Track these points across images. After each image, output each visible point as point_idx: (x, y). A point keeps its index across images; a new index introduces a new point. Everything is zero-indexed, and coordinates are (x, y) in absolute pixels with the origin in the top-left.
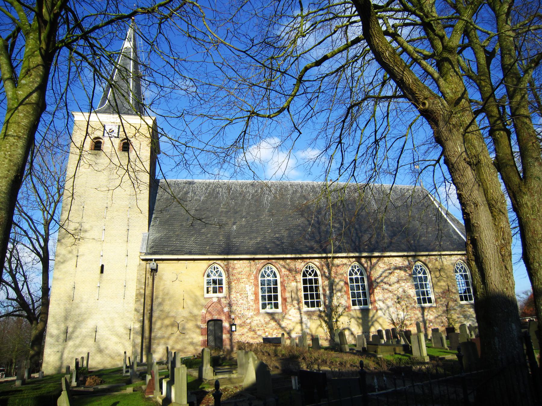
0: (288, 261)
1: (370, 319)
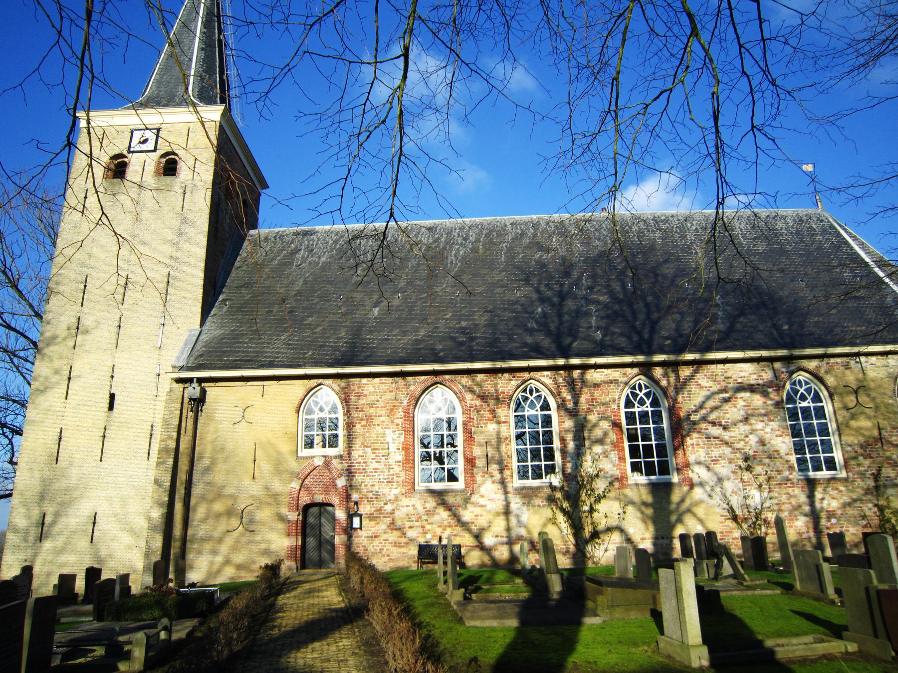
0: (480, 377)
1: (673, 506)
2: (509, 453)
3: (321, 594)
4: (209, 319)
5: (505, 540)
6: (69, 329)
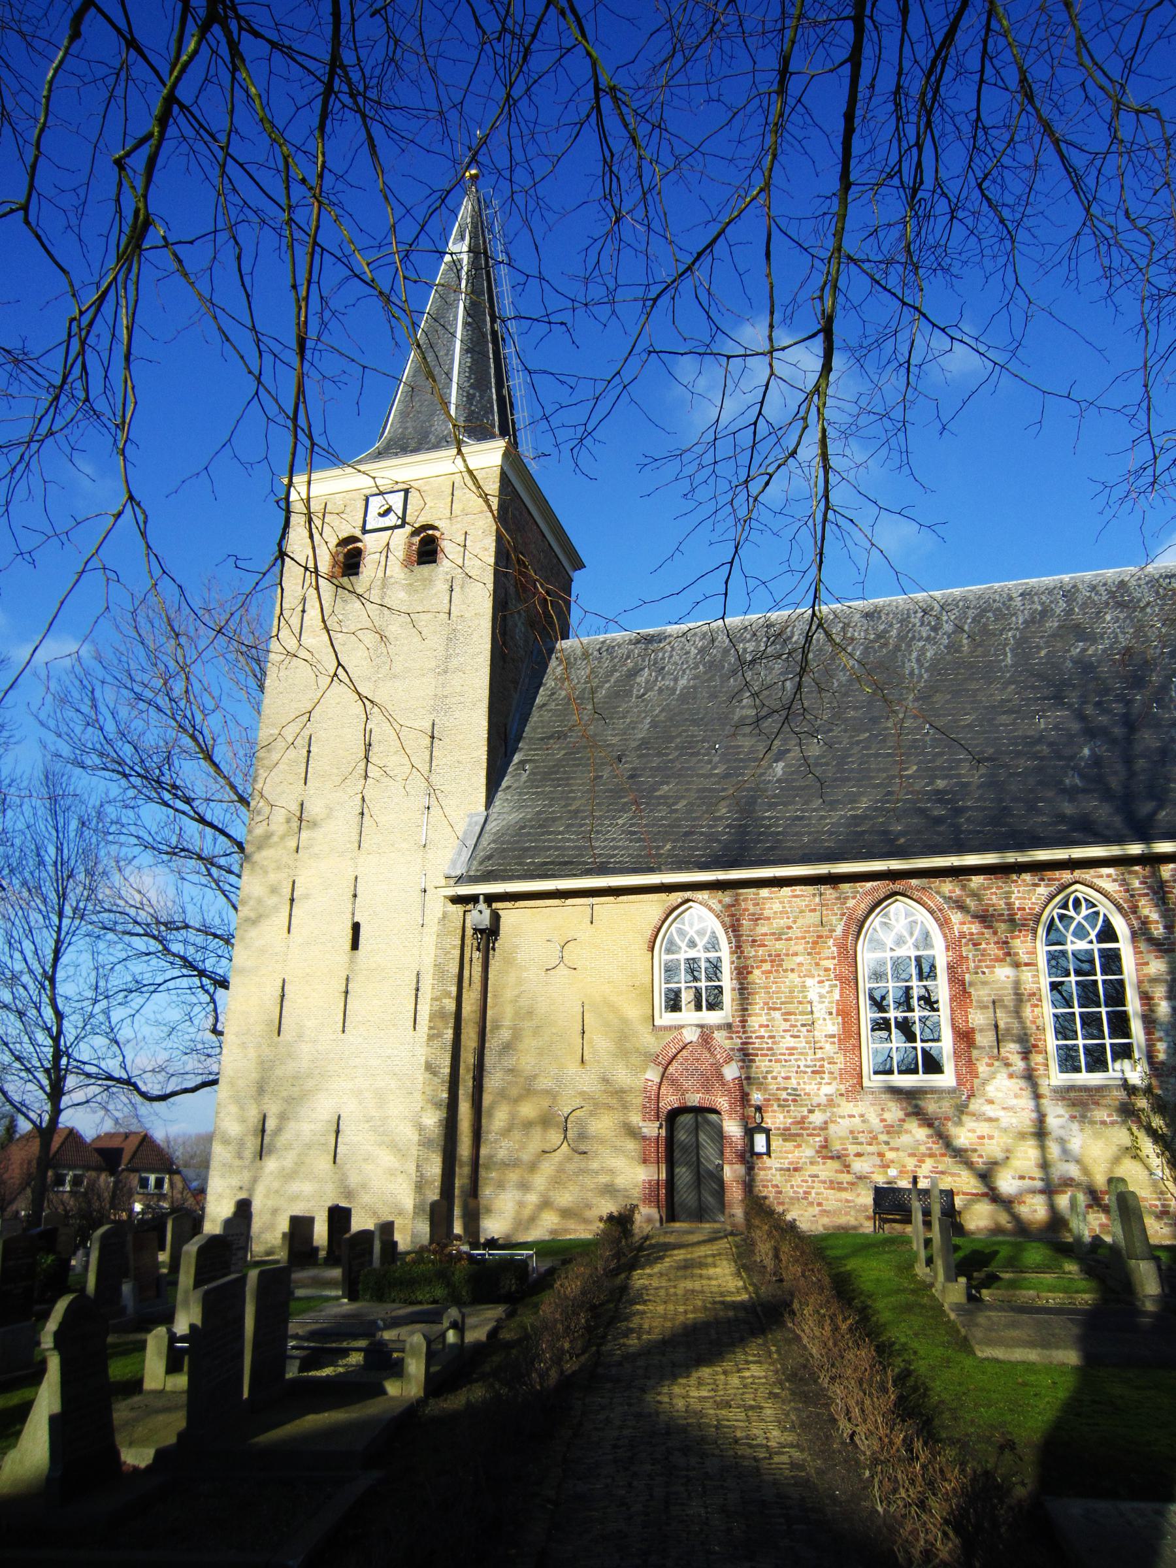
0: (977, 881)
2: (1039, 1022)
3: (704, 1272)
4: (500, 795)
5: (1039, 1184)
6: (288, 821)
